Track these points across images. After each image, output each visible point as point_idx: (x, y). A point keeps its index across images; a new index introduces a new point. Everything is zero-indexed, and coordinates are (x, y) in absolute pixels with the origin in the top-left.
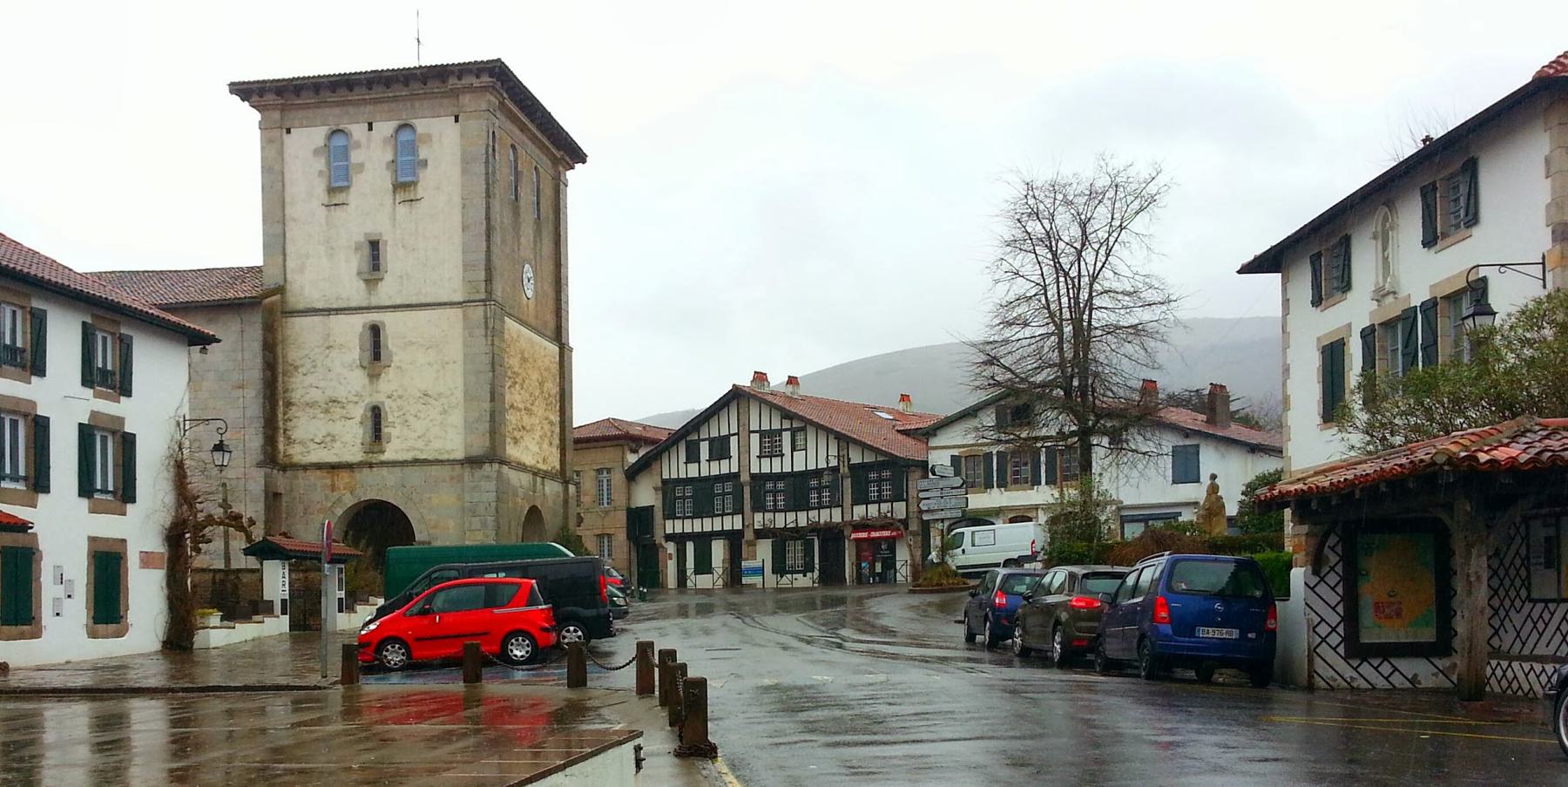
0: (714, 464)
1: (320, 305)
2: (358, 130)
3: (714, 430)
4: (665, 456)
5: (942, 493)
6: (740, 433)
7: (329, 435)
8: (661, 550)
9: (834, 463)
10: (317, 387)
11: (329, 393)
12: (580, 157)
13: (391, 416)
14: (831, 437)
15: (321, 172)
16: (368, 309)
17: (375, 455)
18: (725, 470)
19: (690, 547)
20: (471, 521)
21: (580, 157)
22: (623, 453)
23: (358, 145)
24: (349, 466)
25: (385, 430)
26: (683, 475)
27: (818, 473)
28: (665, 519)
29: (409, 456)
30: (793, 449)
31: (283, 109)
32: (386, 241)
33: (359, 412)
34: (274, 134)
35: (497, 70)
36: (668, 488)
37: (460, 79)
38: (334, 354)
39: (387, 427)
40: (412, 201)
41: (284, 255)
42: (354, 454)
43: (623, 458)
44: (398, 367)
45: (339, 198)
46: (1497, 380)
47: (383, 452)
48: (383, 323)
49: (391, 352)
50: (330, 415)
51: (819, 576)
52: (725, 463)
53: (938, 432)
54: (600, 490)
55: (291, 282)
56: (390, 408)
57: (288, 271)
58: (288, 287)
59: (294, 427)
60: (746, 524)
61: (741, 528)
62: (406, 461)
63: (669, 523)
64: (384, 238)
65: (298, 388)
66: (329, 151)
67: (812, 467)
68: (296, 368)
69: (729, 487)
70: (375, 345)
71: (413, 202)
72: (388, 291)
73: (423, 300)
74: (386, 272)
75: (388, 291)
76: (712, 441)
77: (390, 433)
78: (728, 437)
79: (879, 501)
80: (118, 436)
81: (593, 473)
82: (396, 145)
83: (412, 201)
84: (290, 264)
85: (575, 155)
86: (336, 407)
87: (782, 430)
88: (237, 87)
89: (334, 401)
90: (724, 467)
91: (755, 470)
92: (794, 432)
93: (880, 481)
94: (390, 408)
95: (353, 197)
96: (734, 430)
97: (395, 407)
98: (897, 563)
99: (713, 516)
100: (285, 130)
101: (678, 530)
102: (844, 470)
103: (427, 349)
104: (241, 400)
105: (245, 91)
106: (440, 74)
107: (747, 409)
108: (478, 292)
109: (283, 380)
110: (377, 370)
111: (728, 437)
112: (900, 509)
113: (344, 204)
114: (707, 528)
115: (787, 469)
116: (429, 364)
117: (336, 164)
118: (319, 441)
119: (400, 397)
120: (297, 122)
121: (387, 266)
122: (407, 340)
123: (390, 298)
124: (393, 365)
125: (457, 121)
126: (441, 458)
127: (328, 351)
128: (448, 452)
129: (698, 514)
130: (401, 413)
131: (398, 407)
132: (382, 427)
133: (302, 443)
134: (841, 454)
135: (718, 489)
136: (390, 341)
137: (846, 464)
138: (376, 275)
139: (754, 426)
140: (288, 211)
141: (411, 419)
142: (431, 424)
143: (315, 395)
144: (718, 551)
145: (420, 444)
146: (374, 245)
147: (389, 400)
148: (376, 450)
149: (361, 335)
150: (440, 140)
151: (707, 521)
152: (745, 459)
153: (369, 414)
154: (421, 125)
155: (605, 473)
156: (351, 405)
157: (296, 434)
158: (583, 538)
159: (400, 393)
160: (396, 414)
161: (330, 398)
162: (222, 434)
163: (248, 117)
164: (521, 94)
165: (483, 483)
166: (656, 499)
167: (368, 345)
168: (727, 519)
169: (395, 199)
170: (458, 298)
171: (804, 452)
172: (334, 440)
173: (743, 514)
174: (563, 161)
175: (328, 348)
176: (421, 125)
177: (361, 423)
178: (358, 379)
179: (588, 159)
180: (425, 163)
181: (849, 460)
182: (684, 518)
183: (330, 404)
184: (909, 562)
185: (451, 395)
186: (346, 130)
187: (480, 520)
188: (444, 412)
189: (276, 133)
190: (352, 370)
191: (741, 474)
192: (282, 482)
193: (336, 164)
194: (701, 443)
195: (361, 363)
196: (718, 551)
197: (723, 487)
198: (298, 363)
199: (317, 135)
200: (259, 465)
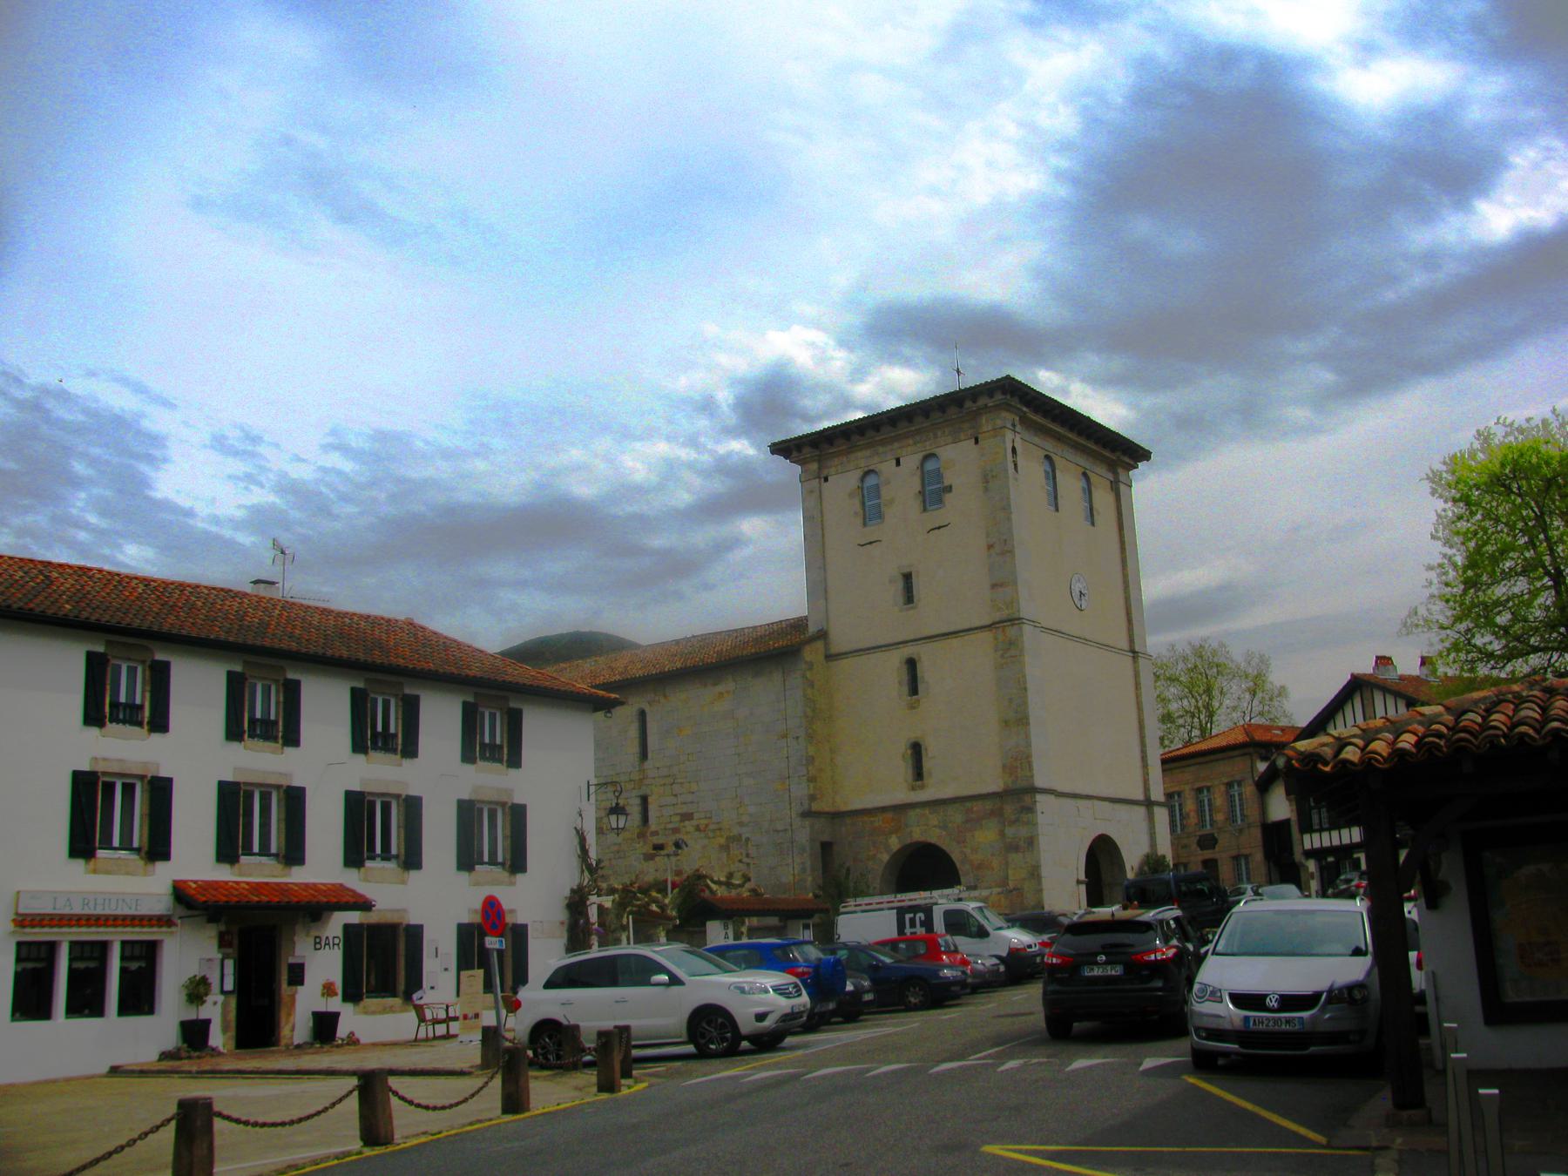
22: (1252, 760)
31: (821, 460)
37: (974, 402)
43: (1252, 768)
46: (727, 838)
54: (1232, 806)
63: (1306, 837)
81: (1223, 788)
88: (777, 447)
100: (823, 480)
101: (1317, 845)
104: (786, 749)
107: (1371, 700)
114: (1346, 841)
120: (833, 470)
136: (924, 670)
146: (908, 578)
155: (1205, 791)
166: (1292, 811)
167: (905, 677)
180: (949, 489)
189: (815, 483)
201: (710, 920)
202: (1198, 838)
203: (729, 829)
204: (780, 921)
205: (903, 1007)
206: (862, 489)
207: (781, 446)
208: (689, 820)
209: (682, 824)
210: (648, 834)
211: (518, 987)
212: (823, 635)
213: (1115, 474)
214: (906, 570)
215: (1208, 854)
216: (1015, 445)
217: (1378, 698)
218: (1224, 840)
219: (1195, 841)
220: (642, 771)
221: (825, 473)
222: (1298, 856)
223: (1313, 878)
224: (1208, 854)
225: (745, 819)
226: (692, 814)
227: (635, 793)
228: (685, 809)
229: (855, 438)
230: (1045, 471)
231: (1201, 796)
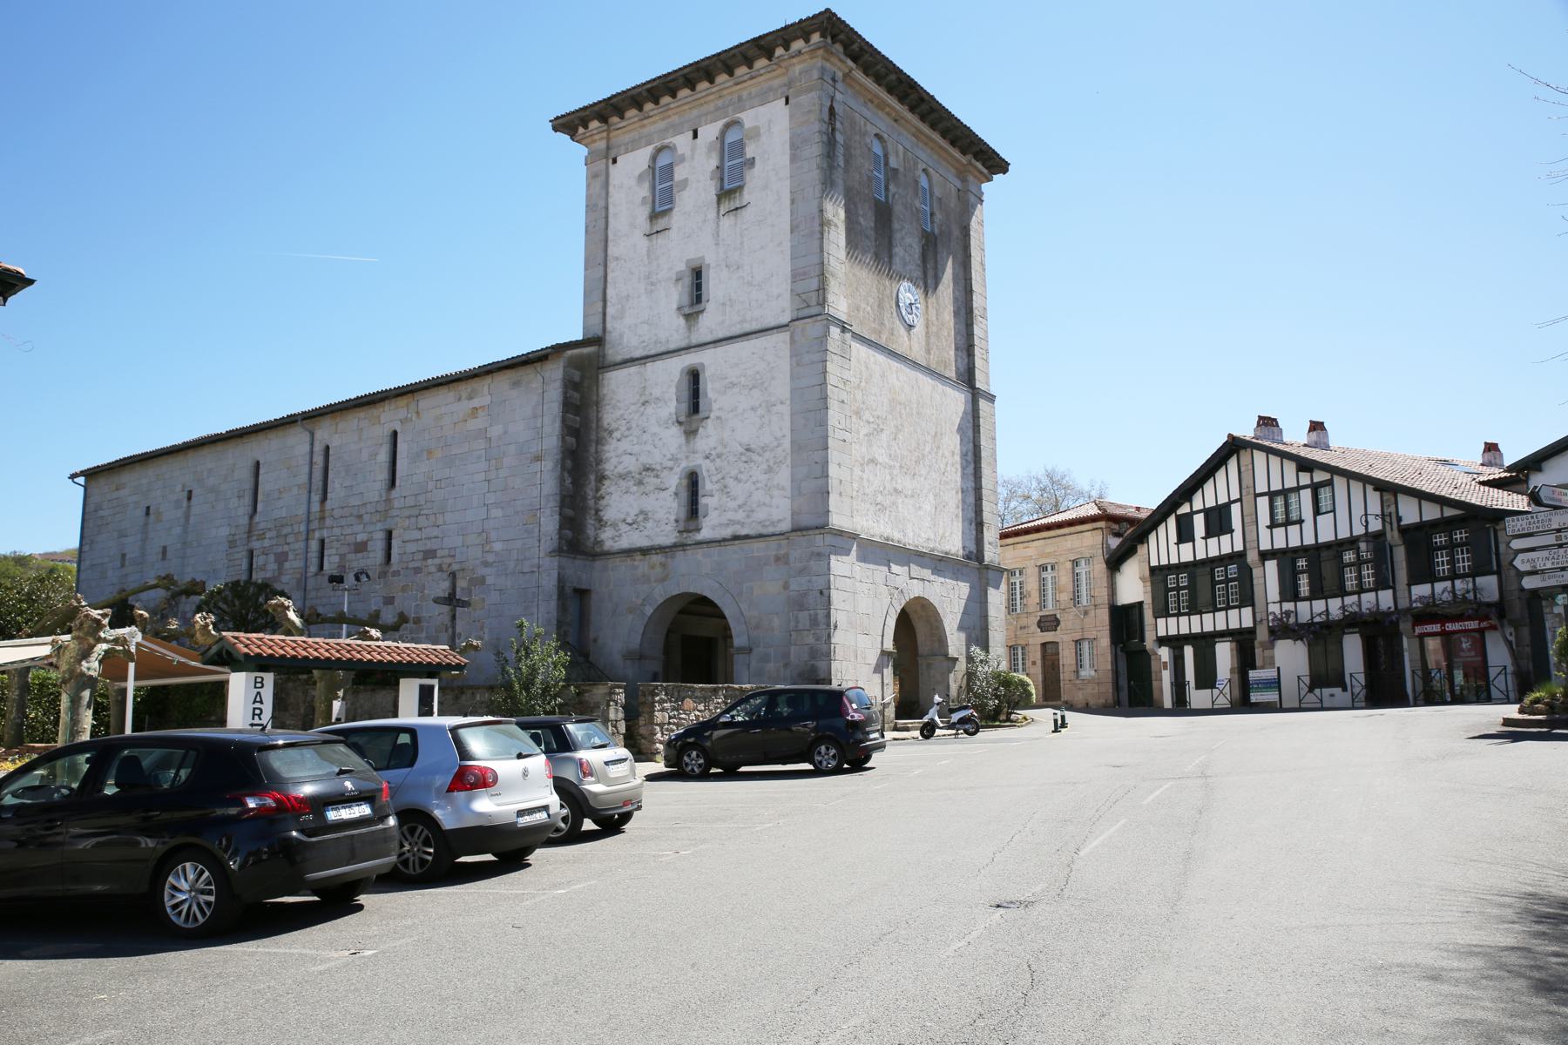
0: (1213, 541)
1: (637, 354)
3: (1208, 497)
4: (1152, 537)
5: (1558, 538)
6: (1243, 498)
7: (642, 512)
8: (1153, 657)
9: (1375, 525)
10: (631, 454)
11: (644, 459)
12: (995, 164)
14: (1369, 488)
16: (688, 348)
17: (690, 534)
18: (1226, 550)
19: (1189, 651)
20: (797, 617)
21: (995, 164)
23: (682, 159)
24: (661, 549)
25: (703, 501)
26: (1174, 561)
27: (1352, 542)
28: (1156, 618)
29: (727, 532)
30: (1317, 511)
32: (709, 265)
33: (674, 480)
36: (1158, 574)
38: (649, 410)
40: (737, 209)
42: (667, 536)
45: (661, 224)
47: (698, 530)
48: (702, 365)
49: (711, 399)
50: (643, 487)
51: (273, 717)
52: (1225, 539)
53: (1544, 465)
55: (610, 332)
56: (706, 469)
57: (608, 318)
58: (607, 338)
59: (607, 506)
60: (1258, 619)
61: (1252, 625)
62: (725, 540)
63: (1161, 622)
65: (611, 457)
67: (1344, 534)
68: (611, 433)
69: (1233, 568)
71: (739, 211)
72: (711, 322)
73: (748, 328)
74: (708, 301)
77: (707, 505)
78: (1227, 506)
79: (1453, 576)
81: (1069, 565)
83: (737, 209)
86: (649, 476)
87: (1298, 489)
89: (648, 469)
92: (1315, 488)
93: (1451, 547)
94: (708, 471)
95: (676, 219)
96: (1235, 495)
97: (713, 469)
98: (1490, 670)
99: (1215, 610)
100: (611, 161)
101: (1173, 632)
102: (1393, 536)
103: (751, 389)
105: (569, 124)
108: (808, 306)
109: (596, 449)
110: (694, 427)
111: (1227, 506)
112: (1489, 585)
113: (666, 229)
114: (1208, 628)
115: (1309, 540)
116: (753, 409)
118: (631, 522)
119: (719, 456)
121: (709, 295)
122: (728, 381)
123: (711, 332)
124: (712, 416)
126: (765, 531)
127: (643, 407)
128: (773, 523)
129: (1194, 609)
130: (719, 476)
131: (717, 469)
133: (614, 525)
134: (1387, 512)
136: (709, 388)
137: (1395, 525)
139: (1261, 487)
140: (612, 250)
141: (730, 482)
142: (753, 487)
143: (630, 464)
144: (1224, 653)
145: (740, 516)
146: (697, 274)
147: (708, 461)
148: (691, 528)
150: (769, 130)
152: (1252, 532)
154: (748, 118)
156: (666, 472)
157: (609, 514)
158: (1060, 644)
159: (720, 449)
160: (715, 479)
161: (644, 465)
163: (572, 154)
164: (876, 64)
165: (812, 563)
166: (1145, 593)
167: (686, 394)
171: (1332, 514)
172: (646, 519)
173: (1253, 605)
174: (971, 168)
175: (643, 404)
176: (748, 118)
177: (676, 494)
179: (1010, 167)
181: (1399, 519)
182: (1179, 615)
183: (644, 473)
184: (1510, 669)
185: (777, 447)
186: (671, 145)
187: (810, 615)
188: (769, 470)
189: (601, 165)
190: (667, 428)
192: (578, 572)
194: (1195, 516)
195: (677, 418)
196: (1224, 653)
197: (1226, 573)
198: (614, 426)
200: (551, 553)
202: (1039, 618)
203: (473, 570)
205: (807, 766)
208: (432, 558)
209: (424, 563)
210: (389, 574)
213: (964, 181)
214: (695, 264)
215: (1049, 636)
216: (835, 105)
217: (1259, 457)
218: (1068, 621)
219: (1036, 622)
220: (388, 501)
222: (1149, 642)
223: (1165, 668)
224: (1049, 636)
225: (490, 558)
226: (435, 551)
227: (380, 526)
228: (429, 545)
231: (1044, 575)
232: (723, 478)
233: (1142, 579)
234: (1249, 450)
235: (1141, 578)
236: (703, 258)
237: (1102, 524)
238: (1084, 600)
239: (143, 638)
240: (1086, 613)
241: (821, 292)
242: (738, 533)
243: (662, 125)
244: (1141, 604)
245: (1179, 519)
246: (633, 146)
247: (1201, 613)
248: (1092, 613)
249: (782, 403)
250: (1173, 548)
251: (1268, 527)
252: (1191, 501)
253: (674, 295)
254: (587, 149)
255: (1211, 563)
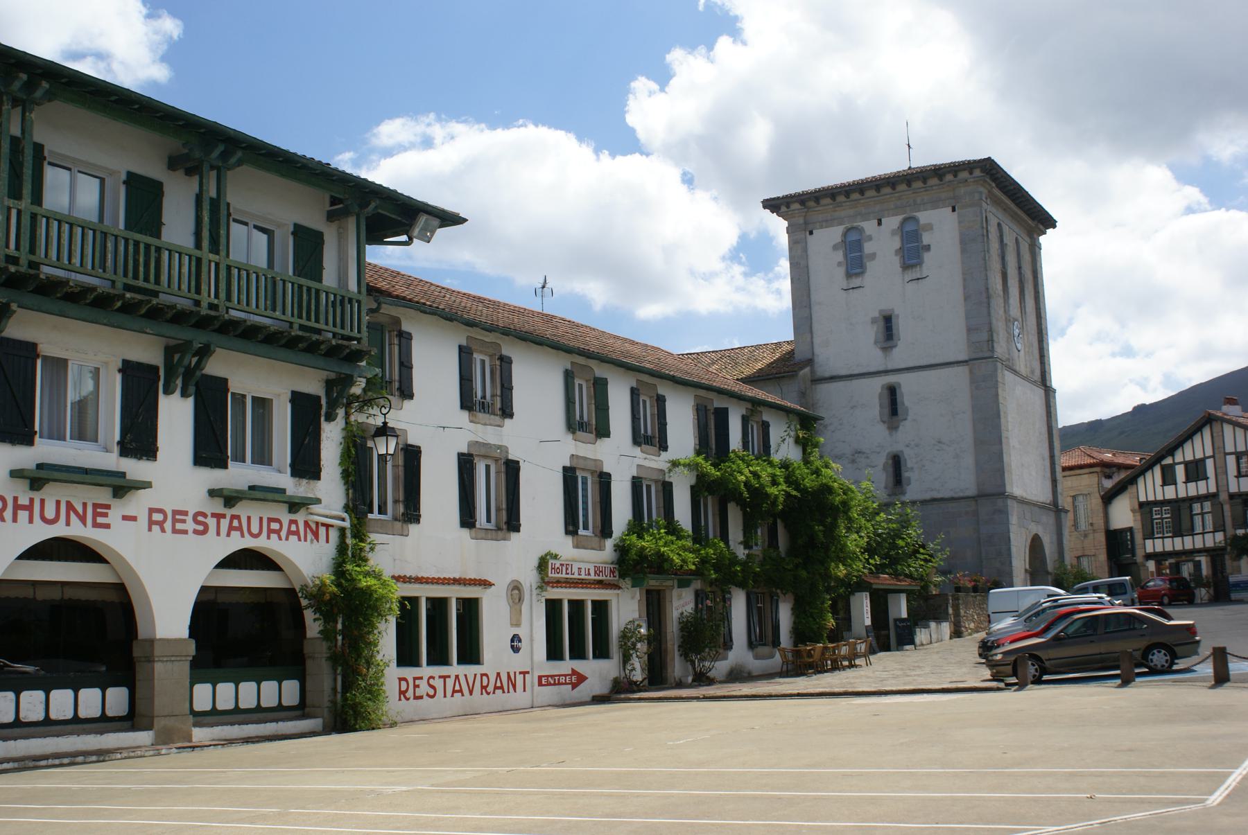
0: (1192, 485)
1: (843, 372)
2: (869, 226)
3: (1188, 452)
4: (1141, 481)
6: (1216, 455)
8: (1141, 568)
12: (1049, 222)
13: (910, 461)
15: (839, 264)
16: (886, 372)
18: (1203, 491)
23: (870, 238)
25: (905, 475)
26: (1160, 498)
28: (1144, 539)
33: (881, 460)
34: (799, 234)
35: (988, 166)
36: (1145, 508)
39: (907, 471)
40: (918, 279)
41: (811, 332)
44: (914, 420)
45: (856, 282)
48: (899, 385)
52: (1202, 484)
55: (818, 355)
58: (816, 360)
63: (1149, 543)
64: (896, 312)
66: (845, 245)
69: (1208, 506)
70: (893, 403)
71: (920, 280)
72: (901, 355)
73: (933, 361)
75: (901, 355)
76: (1187, 464)
78: (1203, 461)
80: (596, 475)
82: (902, 236)
83: (918, 279)
84: (817, 341)
85: (1048, 222)
89: (860, 452)
90: (1201, 488)
91: (1233, 489)
95: (868, 279)
96: (1209, 452)
100: (808, 233)
101: (1159, 549)
106: (938, 172)
111: (1203, 461)
114: (1189, 546)
117: (852, 255)
119: (917, 446)
124: (909, 418)
125: (954, 210)
129: (1178, 532)
132: (902, 471)
135: (1197, 508)
136: (907, 398)
138: (890, 344)
139: (1229, 448)
149: (880, 396)
151: (1188, 540)
153: (890, 462)
154: (924, 217)
162: (385, 415)
166: (1135, 521)
167: (886, 401)
168: (1209, 537)
169: (903, 279)
170: (963, 356)
175: (852, 408)
176: (924, 217)
178: (880, 431)
179: (1057, 224)
180: (928, 248)
183: (856, 455)
191: (1220, 494)
193: (852, 255)
194: (1177, 467)
199: (834, 234)
201: (1156, 563)
204: (340, 630)
206: (845, 242)
207: (773, 203)
211: (193, 686)
212: (810, 362)
217: (1228, 429)
221: (810, 227)
222: (1139, 557)
229: (841, 198)
230: (317, 170)
232: (921, 460)
233: (1133, 511)
234: (1219, 422)
235: (1131, 510)
236: (893, 310)
237: (1098, 469)
238: (1083, 528)
239: (1002, 579)
240: (1086, 536)
241: (990, 342)
242: (935, 497)
243: (851, 212)
244: (1130, 529)
245: (1163, 469)
246: (828, 223)
247: (1182, 536)
248: (1091, 536)
249: (964, 413)
250: (1159, 489)
251: (1236, 477)
252: (1173, 455)
253: (870, 334)
254: (787, 222)
255: (1190, 500)
